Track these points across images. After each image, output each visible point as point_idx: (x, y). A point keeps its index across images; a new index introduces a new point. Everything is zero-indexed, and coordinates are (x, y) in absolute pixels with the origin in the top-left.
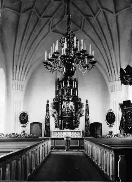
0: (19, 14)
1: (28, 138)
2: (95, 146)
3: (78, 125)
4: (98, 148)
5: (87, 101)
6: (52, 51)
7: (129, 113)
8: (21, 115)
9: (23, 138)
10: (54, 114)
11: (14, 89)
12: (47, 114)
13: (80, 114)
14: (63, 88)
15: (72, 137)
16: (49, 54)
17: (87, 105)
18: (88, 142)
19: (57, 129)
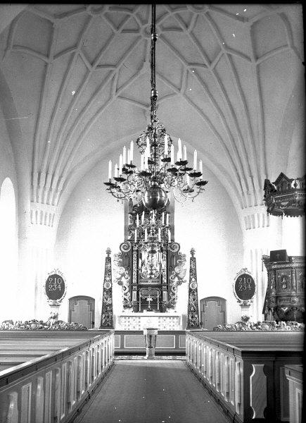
0: (46, 60)
1: (67, 330)
2: (207, 347)
3: (175, 303)
4: (214, 350)
5: (192, 252)
6: (123, 161)
7: (283, 276)
8: (48, 280)
9: (54, 330)
10: (120, 278)
11: (34, 223)
12: (108, 279)
13: (179, 278)
14: (143, 226)
15: (161, 330)
16: (116, 167)
17: (193, 259)
18: (195, 339)
19: (127, 310)
